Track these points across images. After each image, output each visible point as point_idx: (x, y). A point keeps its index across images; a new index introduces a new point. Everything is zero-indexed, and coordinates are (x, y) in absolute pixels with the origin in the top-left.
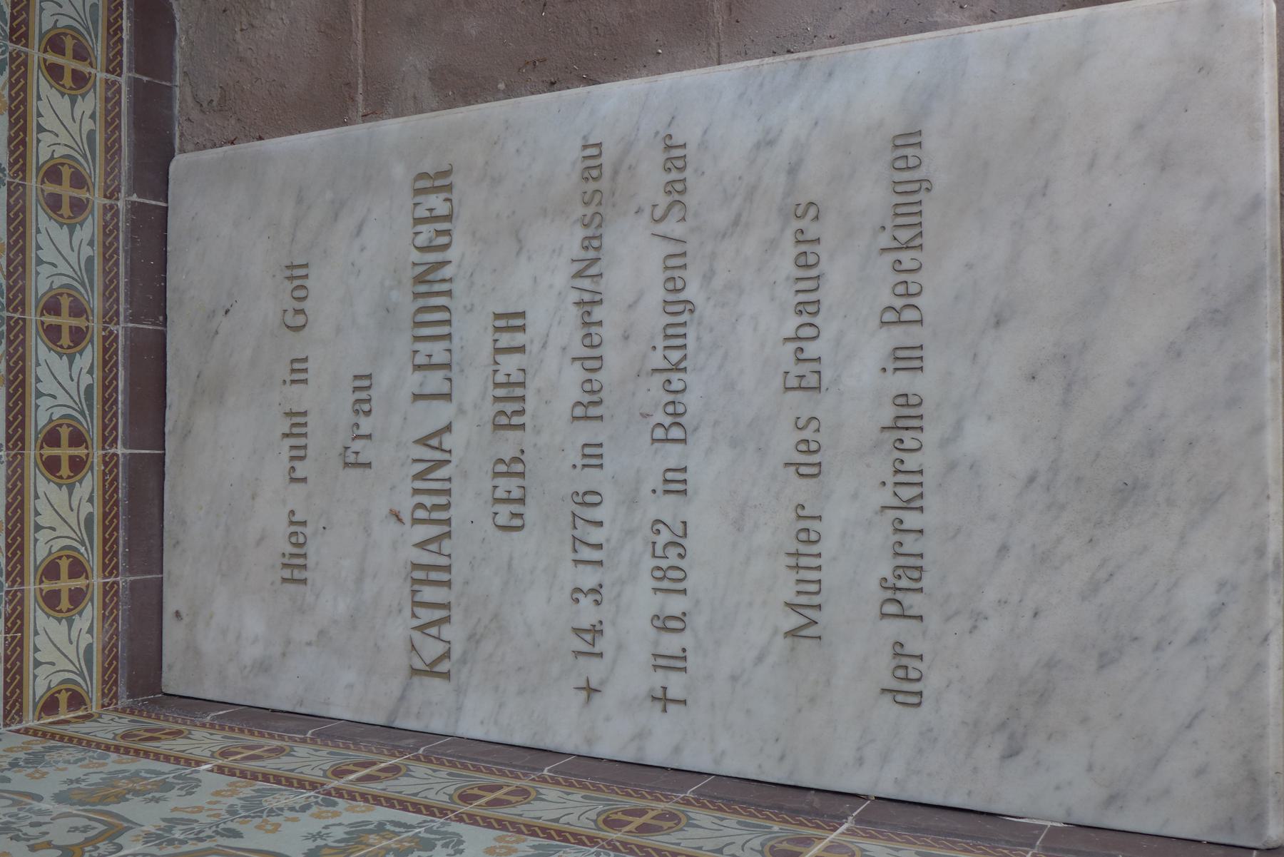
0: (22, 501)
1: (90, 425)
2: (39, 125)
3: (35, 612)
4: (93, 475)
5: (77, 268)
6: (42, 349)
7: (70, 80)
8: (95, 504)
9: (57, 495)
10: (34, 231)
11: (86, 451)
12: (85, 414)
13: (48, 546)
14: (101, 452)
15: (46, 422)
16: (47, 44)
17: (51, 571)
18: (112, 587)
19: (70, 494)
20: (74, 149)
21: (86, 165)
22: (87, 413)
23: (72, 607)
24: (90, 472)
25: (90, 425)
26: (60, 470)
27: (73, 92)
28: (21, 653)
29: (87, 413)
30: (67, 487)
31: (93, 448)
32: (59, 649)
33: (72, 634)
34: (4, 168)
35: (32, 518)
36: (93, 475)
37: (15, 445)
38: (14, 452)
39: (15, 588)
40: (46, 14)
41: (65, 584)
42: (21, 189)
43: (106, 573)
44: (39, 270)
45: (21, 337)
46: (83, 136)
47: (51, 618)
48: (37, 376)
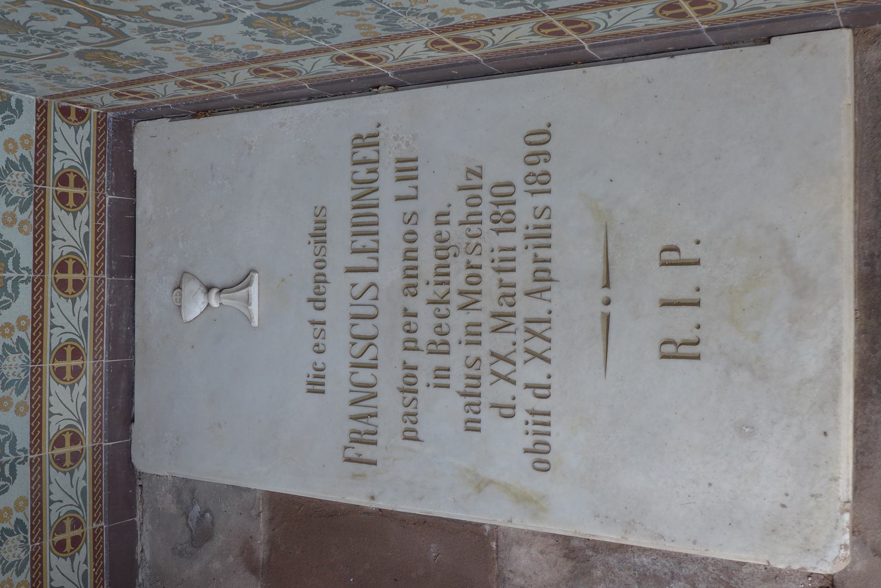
0: (41, 407)
1: (88, 174)
2: (50, 412)
3: (54, 116)
4: (91, 123)
5: (75, 413)
6: (58, 120)
7: (73, 202)
8: (90, 226)
9: (64, 564)
10: (49, 305)
11: (84, 191)
12: (84, 252)
13: (58, 512)
14: (92, 362)
15: (57, 518)
16: (57, 181)
17: (60, 354)
18: (98, 448)
19: (76, 132)
20: (75, 247)
21: (84, 172)
22: (85, 252)
23: (73, 548)
24: (84, 375)
25: (88, 174)
26: (67, 288)
27: (74, 210)
28: (41, 442)
29: (85, 252)
30: (69, 473)
31: (89, 191)
32: (66, 318)
33: (73, 480)
34: (27, 449)
35: (50, 232)
36: (91, 123)
37: (39, 272)
38: (38, 276)
39: (37, 366)
40: (56, 249)
41: (70, 276)
42: (43, 192)
43: (97, 272)
44: (50, 420)
45: (43, 227)
46: (81, 236)
47: (63, 210)
48: (53, 227)
